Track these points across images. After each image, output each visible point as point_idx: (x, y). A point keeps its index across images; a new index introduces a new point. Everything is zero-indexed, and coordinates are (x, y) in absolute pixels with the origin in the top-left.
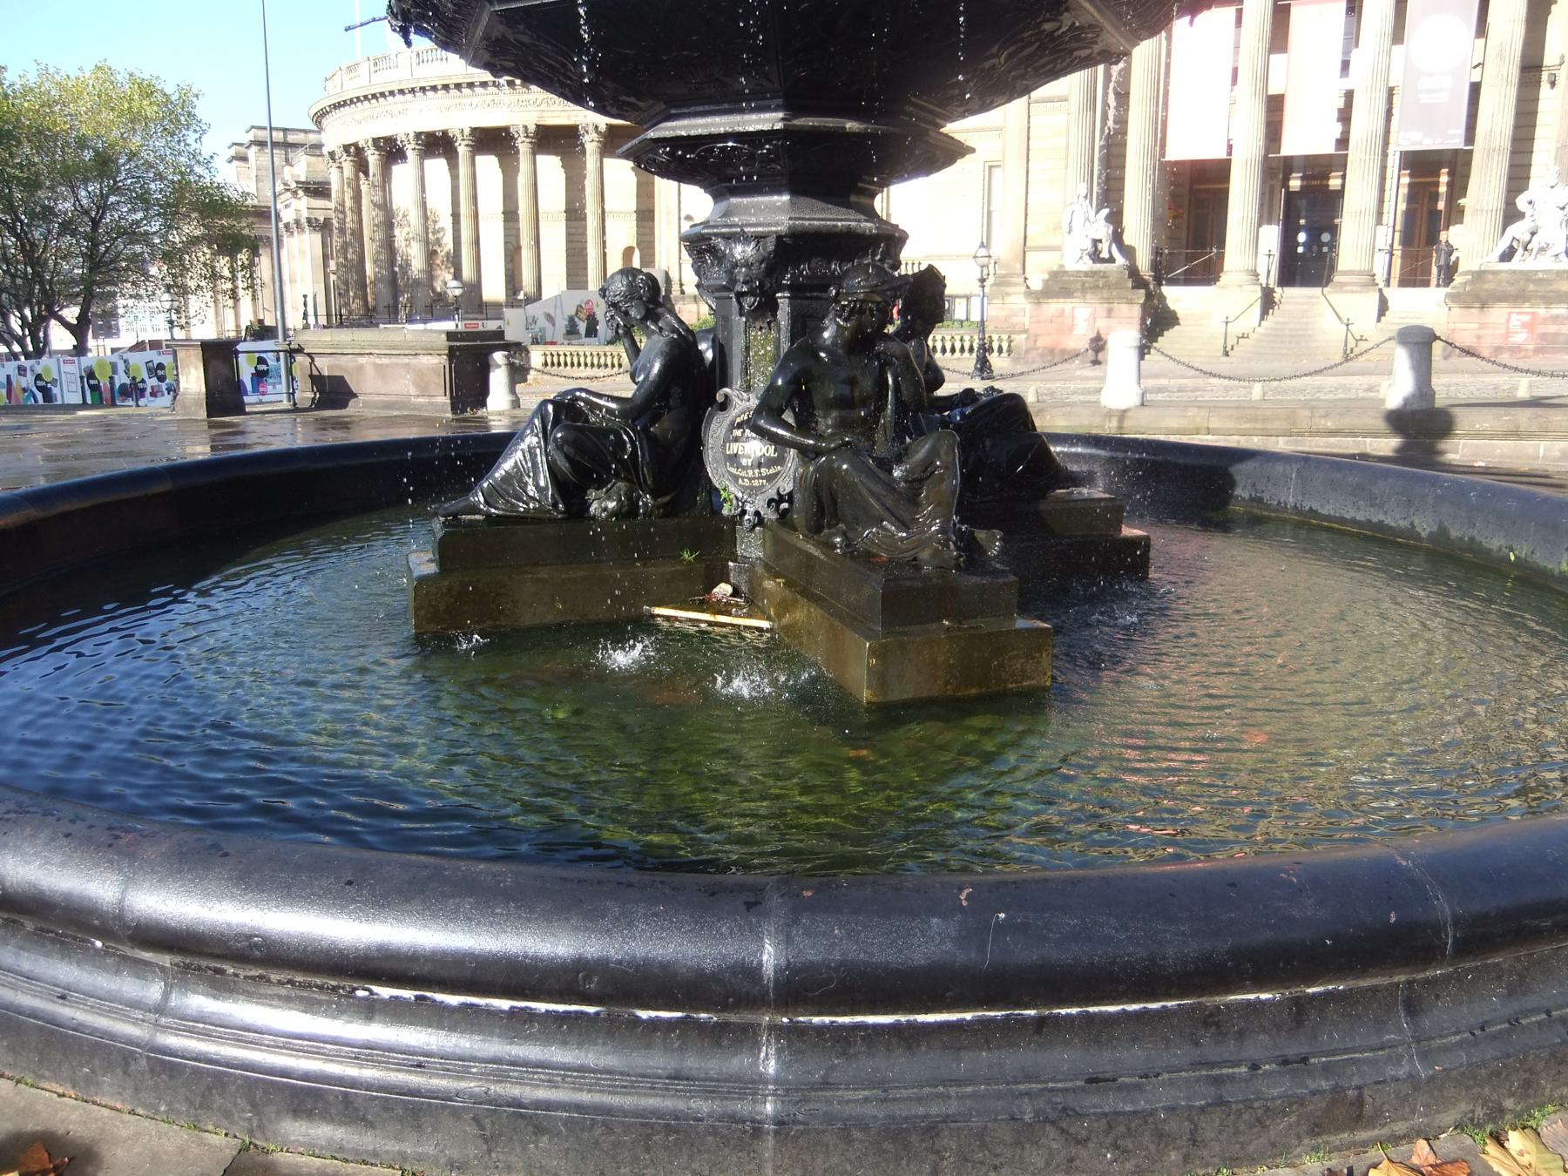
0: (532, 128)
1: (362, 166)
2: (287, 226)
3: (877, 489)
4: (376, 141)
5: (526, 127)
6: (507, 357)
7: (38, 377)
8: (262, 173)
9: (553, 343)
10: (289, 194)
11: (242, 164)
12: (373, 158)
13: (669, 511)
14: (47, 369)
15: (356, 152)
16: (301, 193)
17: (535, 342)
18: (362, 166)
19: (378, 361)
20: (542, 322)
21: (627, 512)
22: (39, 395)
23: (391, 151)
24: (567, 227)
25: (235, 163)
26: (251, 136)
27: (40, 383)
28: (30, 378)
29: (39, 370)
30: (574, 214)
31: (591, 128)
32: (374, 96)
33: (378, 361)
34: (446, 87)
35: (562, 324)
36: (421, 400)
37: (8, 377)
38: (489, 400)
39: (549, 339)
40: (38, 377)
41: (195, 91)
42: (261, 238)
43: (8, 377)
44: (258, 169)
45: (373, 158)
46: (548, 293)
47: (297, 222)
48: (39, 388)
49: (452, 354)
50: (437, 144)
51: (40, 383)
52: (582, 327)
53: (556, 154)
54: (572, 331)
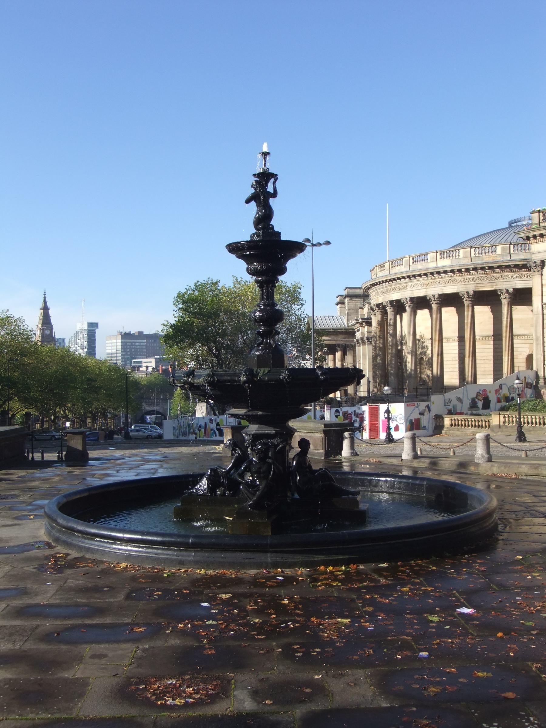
0: (471, 293)
1: (384, 313)
2: (358, 341)
3: (246, 492)
4: (391, 302)
5: (468, 293)
6: (350, 434)
7: (218, 424)
8: (351, 311)
9: (461, 414)
10: (358, 325)
11: (342, 306)
12: (390, 311)
13: (234, 495)
14: (222, 420)
15: (382, 308)
16: (364, 324)
17: (450, 413)
18: (384, 313)
19: (301, 434)
20: (455, 402)
21: (223, 494)
22: (217, 433)
23: (399, 307)
24: (494, 344)
25: (339, 305)
26: (345, 293)
27: (218, 427)
28: (214, 424)
29: (218, 421)
30: (497, 337)
31: (504, 291)
32: (390, 280)
33: (301, 434)
34: (426, 274)
35: (467, 403)
36: (315, 451)
37: (206, 423)
38: (343, 452)
39: (459, 411)
40: (218, 424)
41: (299, 285)
42: (348, 346)
43: (206, 423)
44: (349, 309)
45: (390, 311)
46: (481, 381)
47: (362, 339)
48: (218, 429)
49: (325, 432)
50: (421, 303)
51: (218, 427)
52: (480, 404)
53: (488, 305)
54: (473, 405)
